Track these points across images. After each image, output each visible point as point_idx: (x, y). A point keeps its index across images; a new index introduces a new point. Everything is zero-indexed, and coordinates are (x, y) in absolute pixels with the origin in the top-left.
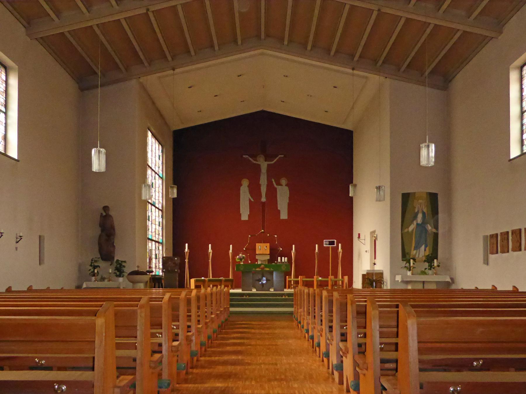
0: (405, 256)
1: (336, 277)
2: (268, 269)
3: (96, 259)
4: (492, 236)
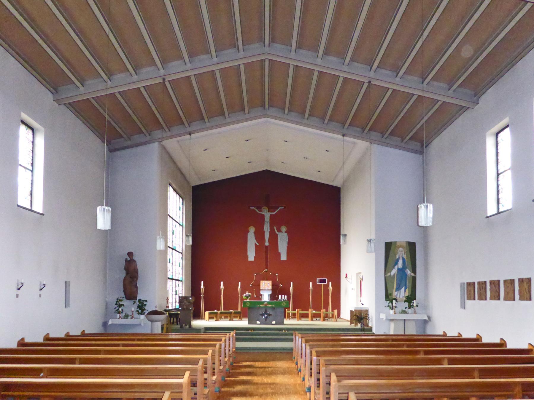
0: (388, 297)
1: (327, 310)
2: (270, 306)
3: (121, 299)
4: (469, 284)
